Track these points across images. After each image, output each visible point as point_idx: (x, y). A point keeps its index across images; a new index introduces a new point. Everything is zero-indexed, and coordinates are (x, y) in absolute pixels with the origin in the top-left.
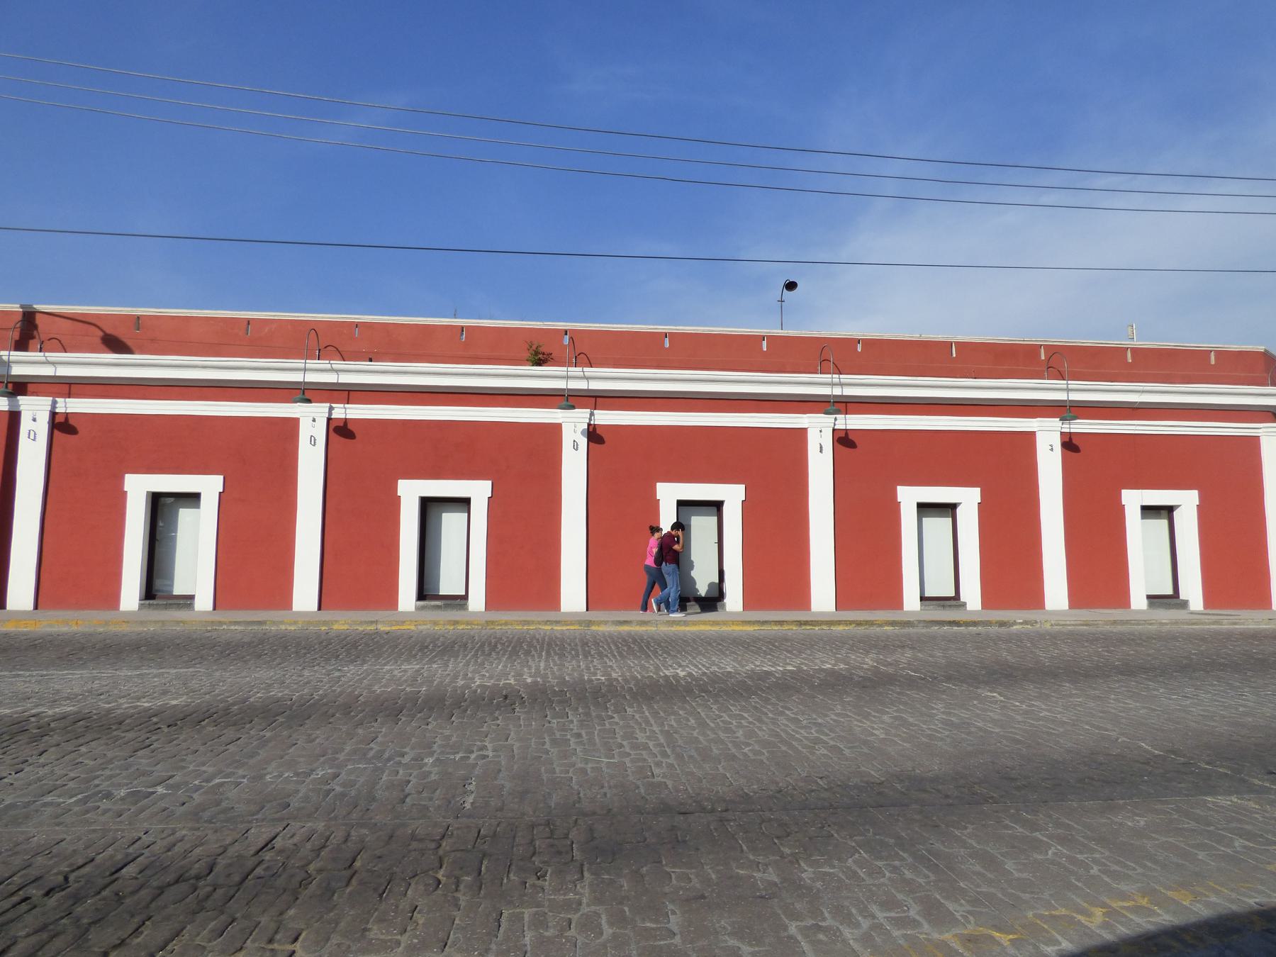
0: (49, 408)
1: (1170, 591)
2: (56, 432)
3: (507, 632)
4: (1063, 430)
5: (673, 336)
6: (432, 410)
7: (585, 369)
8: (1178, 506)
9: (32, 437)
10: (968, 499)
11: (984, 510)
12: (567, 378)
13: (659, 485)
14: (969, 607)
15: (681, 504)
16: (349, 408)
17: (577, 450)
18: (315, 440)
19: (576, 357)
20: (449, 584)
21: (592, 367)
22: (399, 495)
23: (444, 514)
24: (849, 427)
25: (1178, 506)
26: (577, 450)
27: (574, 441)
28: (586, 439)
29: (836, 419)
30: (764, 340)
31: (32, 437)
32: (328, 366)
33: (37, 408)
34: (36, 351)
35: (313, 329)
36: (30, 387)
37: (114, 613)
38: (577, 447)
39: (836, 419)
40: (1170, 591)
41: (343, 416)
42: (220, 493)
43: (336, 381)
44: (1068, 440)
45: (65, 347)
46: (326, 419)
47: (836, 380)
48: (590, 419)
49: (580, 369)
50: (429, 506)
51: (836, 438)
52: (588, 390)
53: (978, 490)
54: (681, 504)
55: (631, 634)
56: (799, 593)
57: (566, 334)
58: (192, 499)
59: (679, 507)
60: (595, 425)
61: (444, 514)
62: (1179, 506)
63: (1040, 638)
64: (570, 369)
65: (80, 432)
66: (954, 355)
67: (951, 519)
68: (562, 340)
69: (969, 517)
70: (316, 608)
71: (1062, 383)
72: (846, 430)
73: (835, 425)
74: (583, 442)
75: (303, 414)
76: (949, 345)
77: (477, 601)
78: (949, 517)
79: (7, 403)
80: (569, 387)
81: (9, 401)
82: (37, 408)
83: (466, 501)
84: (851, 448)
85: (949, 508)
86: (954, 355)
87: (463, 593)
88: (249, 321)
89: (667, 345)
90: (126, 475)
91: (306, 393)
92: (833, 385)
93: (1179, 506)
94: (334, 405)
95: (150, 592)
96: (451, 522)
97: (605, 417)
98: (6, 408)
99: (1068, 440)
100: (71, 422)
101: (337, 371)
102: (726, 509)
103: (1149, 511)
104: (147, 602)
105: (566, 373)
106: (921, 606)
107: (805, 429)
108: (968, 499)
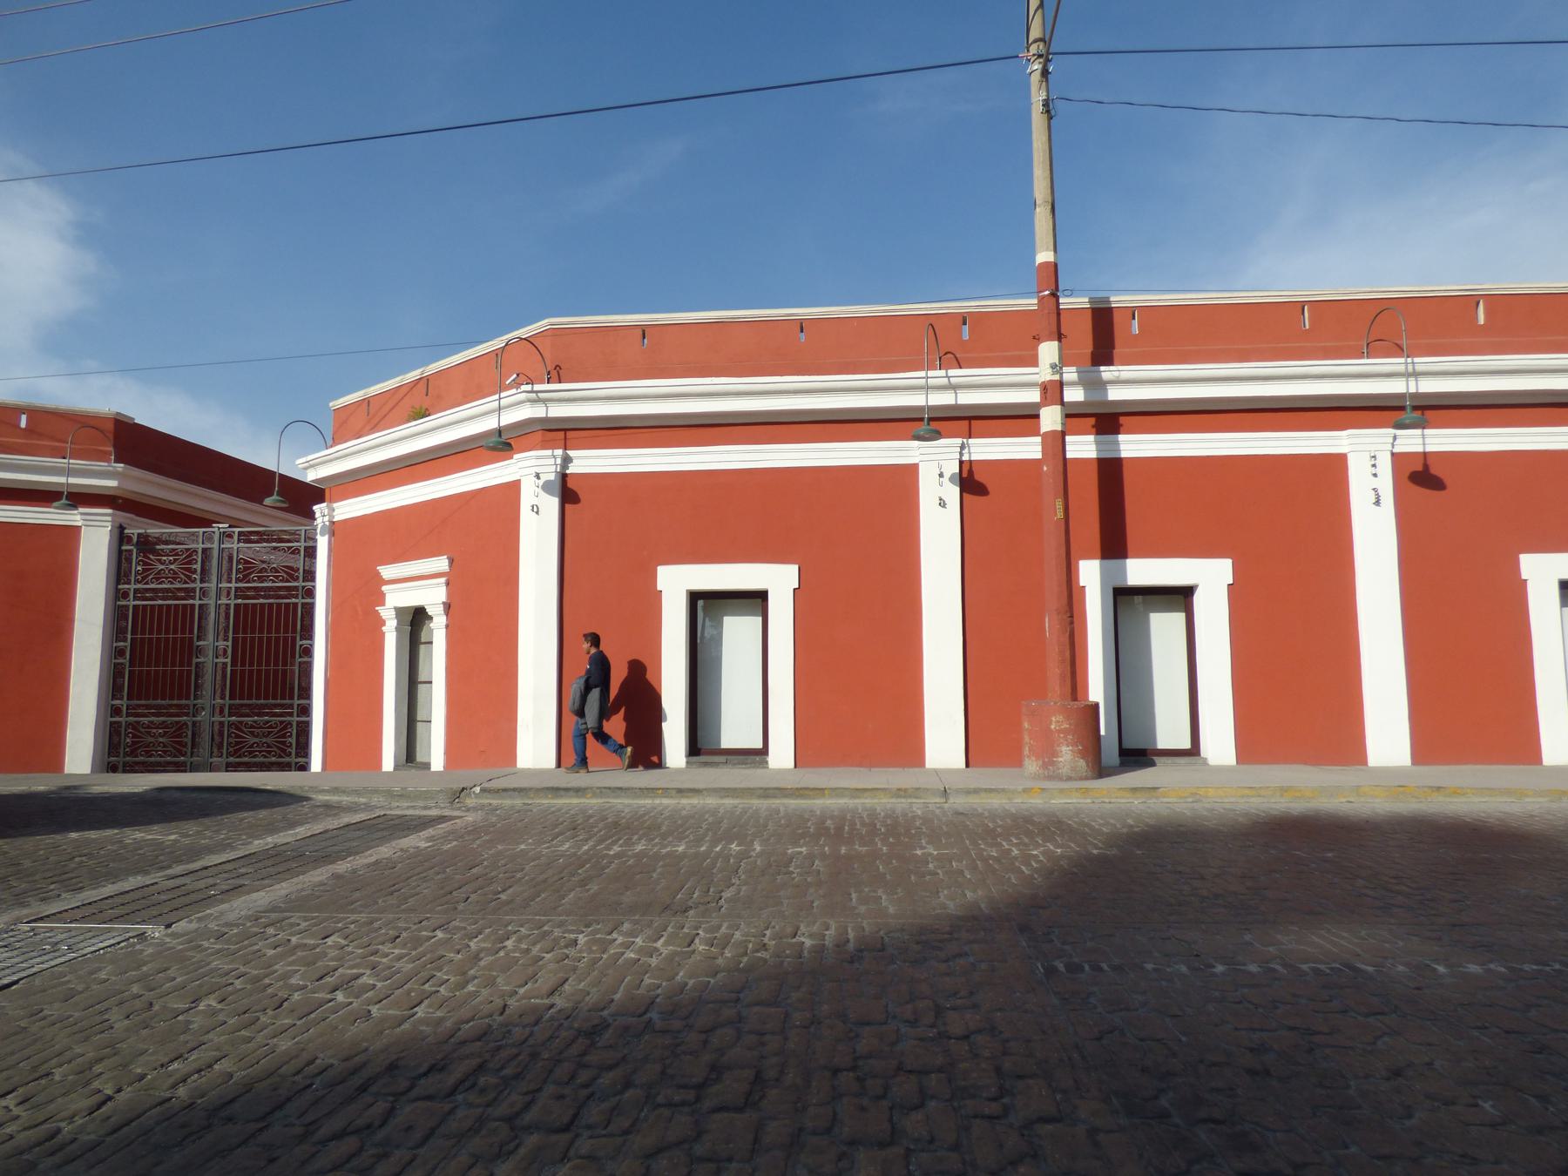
1: (1186, 744)
2: (964, 494)
7: (952, 372)
9: (535, 510)
11: (1236, 593)
12: (927, 388)
14: (434, 768)
15: (695, 597)
19: (940, 358)
20: (736, 730)
21: (961, 368)
22: (659, 589)
23: (725, 618)
24: (1429, 449)
27: (941, 499)
28: (958, 489)
29: (1395, 438)
30: (1134, 318)
31: (535, 510)
33: (944, 456)
36: (1122, 420)
37: (759, 771)
39: (1395, 438)
40: (1186, 744)
41: (1420, 449)
42: (795, 589)
43: (954, 403)
45: (960, 361)
48: (961, 454)
50: (704, 604)
54: (695, 597)
55: (894, 812)
57: (965, 323)
58: (756, 600)
60: (970, 461)
61: (725, 618)
63: (899, 830)
64: (931, 373)
65: (1406, 480)
66: (1307, 327)
69: (1213, 610)
70: (963, 765)
71: (1396, 363)
72: (1425, 454)
73: (1393, 446)
74: (953, 493)
76: (1471, 301)
77: (782, 755)
79: (1122, 447)
80: (959, 402)
81: (1097, 443)
82: (944, 456)
85: (1181, 594)
86: (1307, 327)
87: (759, 745)
88: (644, 331)
91: (502, 444)
94: (572, 453)
95: (694, 749)
96: (738, 631)
97: (589, 461)
98: (1093, 455)
100: (1434, 470)
104: (695, 759)
106: (687, 762)
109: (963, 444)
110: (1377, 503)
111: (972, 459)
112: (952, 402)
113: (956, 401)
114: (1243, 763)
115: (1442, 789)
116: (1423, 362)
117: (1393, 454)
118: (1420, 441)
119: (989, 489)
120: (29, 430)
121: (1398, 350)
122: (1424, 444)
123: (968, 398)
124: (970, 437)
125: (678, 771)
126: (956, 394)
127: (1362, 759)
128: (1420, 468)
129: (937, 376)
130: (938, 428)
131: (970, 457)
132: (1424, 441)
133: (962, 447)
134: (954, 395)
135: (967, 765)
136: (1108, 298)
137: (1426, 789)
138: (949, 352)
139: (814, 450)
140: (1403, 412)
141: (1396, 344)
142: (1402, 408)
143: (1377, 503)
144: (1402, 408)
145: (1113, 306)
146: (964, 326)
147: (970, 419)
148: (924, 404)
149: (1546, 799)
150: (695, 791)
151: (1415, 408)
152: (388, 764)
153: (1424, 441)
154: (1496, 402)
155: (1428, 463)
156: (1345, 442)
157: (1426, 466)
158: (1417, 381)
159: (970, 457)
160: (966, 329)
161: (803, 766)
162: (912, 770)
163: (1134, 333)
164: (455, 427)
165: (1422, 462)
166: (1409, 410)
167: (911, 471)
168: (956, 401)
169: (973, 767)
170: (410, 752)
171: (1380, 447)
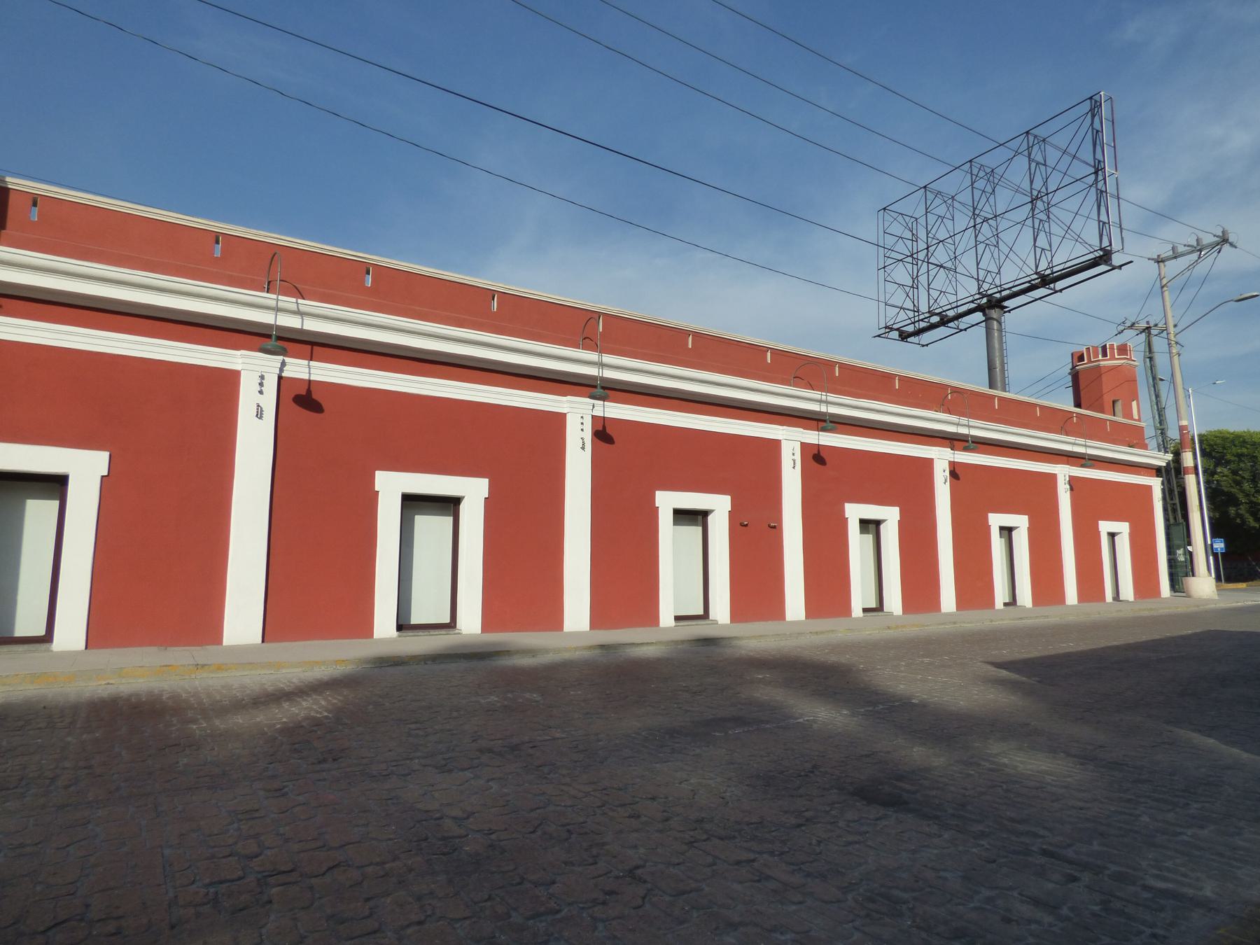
0: (277, 371)
3: (244, 700)
4: (595, 413)
5: (1043, 408)
6: (915, 448)
8: (712, 511)
10: (719, 505)
11: (491, 505)
13: (378, 473)
16: (316, 368)
17: (261, 418)
18: (262, 411)
22: (657, 505)
23: (416, 517)
24: (956, 460)
25: (712, 511)
26: (261, 418)
27: (258, 406)
30: (493, 299)
32: (1084, 443)
34: (262, 291)
35: (275, 252)
38: (261, 414)
41: (306, 377)
44: (601, 429)
46: (277, 376)
47: (824, 398)
48: (281, 370)
49: (274, 296)
51: (594, 431)
52: (301, 331)
53: (486, 481)
56: (1060, 597)
57: (35, 204)
59: (404, 502)
62: (1017, 527)
65: (292, 401)
67: (452, 518)
68: (363, 281)
71: (592, 356)
72: (310, 381)
75: (246, 367)
76: (683, 333)
78: (450, 516)
80: (304, 328)
83: (704, 514)
84: (820, 464)
89: (369, 281)
90: (729, 497)
92: (821, 401)
93: (1017, 527)
99: (601, 429)
101: (827, 402)
102: (464, 508)
103: (682, 516)
105: (275, 302)
107: (565, 415)
108: (719, 505)
109: (284, 361)
110: (583, 448)
111: (312, 379)
112: (299, 327)
113: (276, 321)
114: (599, 628)
115: (206, 667)
116: (608, 359)
117: (280, 378)
118: (307, 370)
119: (615, 440)
120: (374, 291)
121: (593, 347)
122: (310, 373)
123: (312, 325)
124: (311, 360)
125: (857, 619)
126: (303, 319)
127: (1105, 601)
128: (303, 392)
129: (288, 302)
130: (285, 347)
131: (310, 376)
132: (310, 371)
133: (283, 364)
134: (301, 320)
135: (263, 641)
136: (4, 177)
137: (191, 667)
138: (588, 338)
139: (401, 380)
140: (268, 340)
141: (295, 286)
142: (269, 336)
143: (583, 448)
144: (269, 336)
145: (10, 187)
146: (367, 275)
147: (313, 344)
148: (273, 323)
149: (300, 669)
150: (822, 633)
151: (279, 338)
152: (999, 604)
153: (310, 371)
154: (76, 303)
155: (311, 389)
156: (240, 361)
157: (309, 391)
158: (303, 319)
159: (310, 376)
160: (35, 211)
161: (271, 641)
162: (847, 618)
163: (32, 219)
164: (436, 339)
165: (307, 387)
166: (828, 421)
167: (777, 443)
168: (276, 321)
169: (267, 642)
170: (1117, 597)
171: (585, 412)
